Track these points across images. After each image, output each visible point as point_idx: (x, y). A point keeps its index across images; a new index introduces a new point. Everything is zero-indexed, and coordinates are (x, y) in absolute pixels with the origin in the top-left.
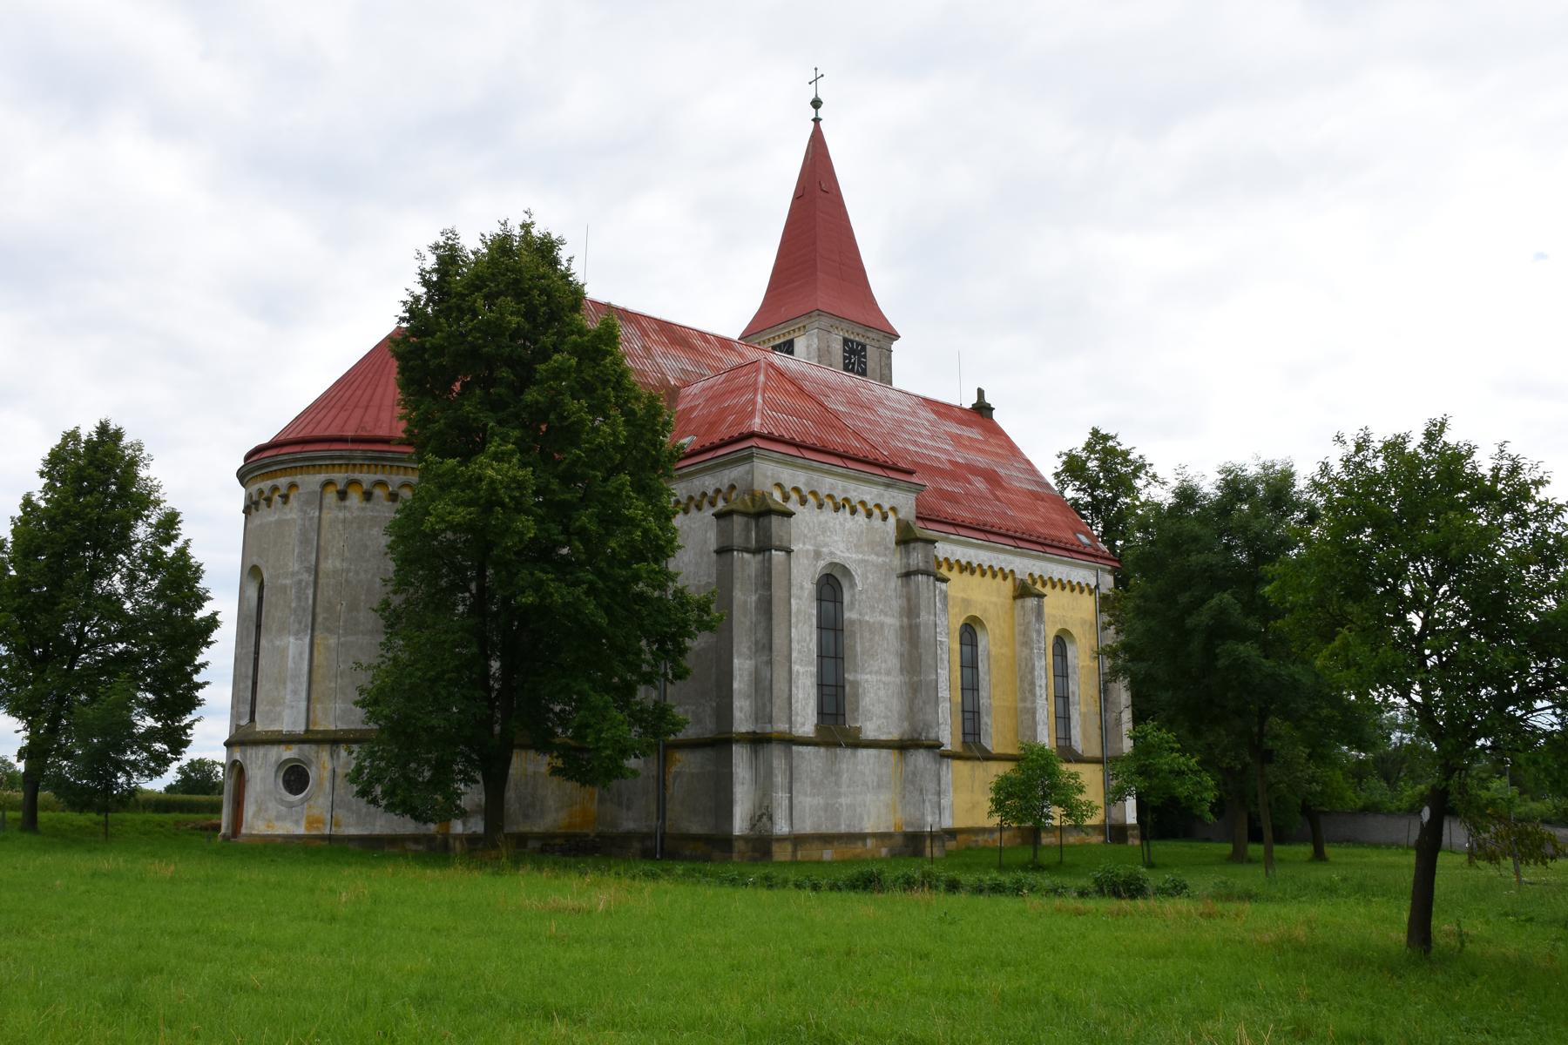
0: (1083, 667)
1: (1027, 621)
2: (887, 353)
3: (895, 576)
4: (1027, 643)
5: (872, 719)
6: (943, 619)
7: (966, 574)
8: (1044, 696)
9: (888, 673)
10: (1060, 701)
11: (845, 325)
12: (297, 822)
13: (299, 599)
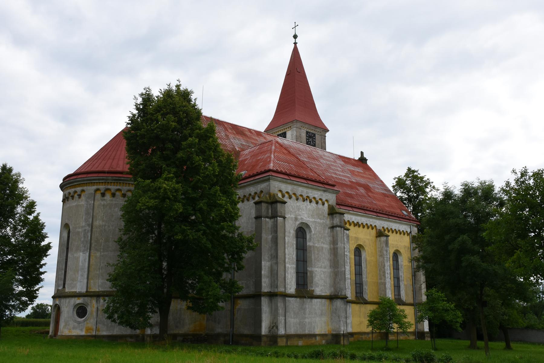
0: (405, 266)
1: (382, 246)
3: (328, 228)
5: (318, 287)
7: (357, 227)
8: (389, 278)
9: (325, 268)
10: (396, 280)
11: (307, 126)
12: (82, 330)
13: (85, 237)
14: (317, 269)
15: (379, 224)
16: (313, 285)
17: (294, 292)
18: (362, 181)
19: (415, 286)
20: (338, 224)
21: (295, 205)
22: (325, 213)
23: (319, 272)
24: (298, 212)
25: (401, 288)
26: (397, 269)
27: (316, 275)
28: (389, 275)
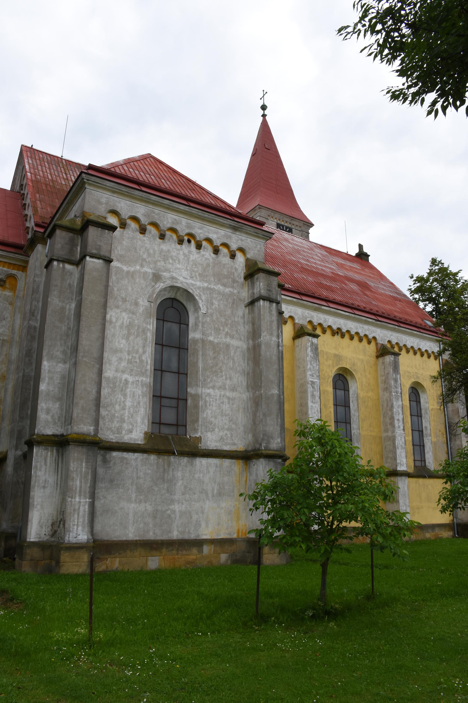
0: (432, 409)
1: (386, 372)
2: (306, 234)
3: (243, 306)
4: (387, 389)
5: (214, 430)
6: (315, 365)
7: (338, 338)
8: (402, 427)
9: (233, 389)
10: (416, 434)
11: (277, 216)
14: (211, 390)
15: (381, 335)
16: (198, 426)
17: (141, 441)
18: (357, 277)
19: (452, 445)
20: (264, 293)
21: (156, 248)
22: (236, 274)
23: (218, 397)
24: (162, 263)
25: (425, 448)
26: (418, 416)
27: (208, 404)
28: (401, 424)
